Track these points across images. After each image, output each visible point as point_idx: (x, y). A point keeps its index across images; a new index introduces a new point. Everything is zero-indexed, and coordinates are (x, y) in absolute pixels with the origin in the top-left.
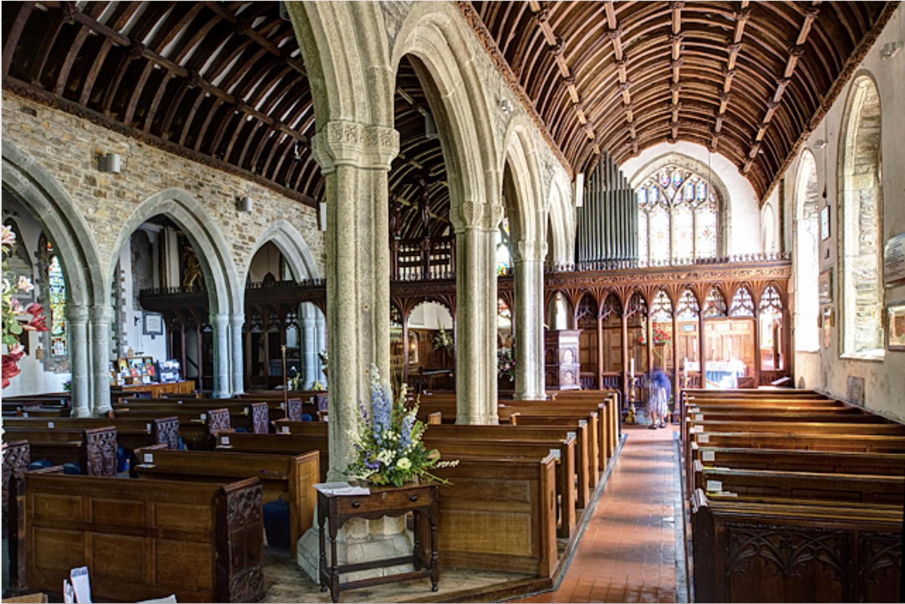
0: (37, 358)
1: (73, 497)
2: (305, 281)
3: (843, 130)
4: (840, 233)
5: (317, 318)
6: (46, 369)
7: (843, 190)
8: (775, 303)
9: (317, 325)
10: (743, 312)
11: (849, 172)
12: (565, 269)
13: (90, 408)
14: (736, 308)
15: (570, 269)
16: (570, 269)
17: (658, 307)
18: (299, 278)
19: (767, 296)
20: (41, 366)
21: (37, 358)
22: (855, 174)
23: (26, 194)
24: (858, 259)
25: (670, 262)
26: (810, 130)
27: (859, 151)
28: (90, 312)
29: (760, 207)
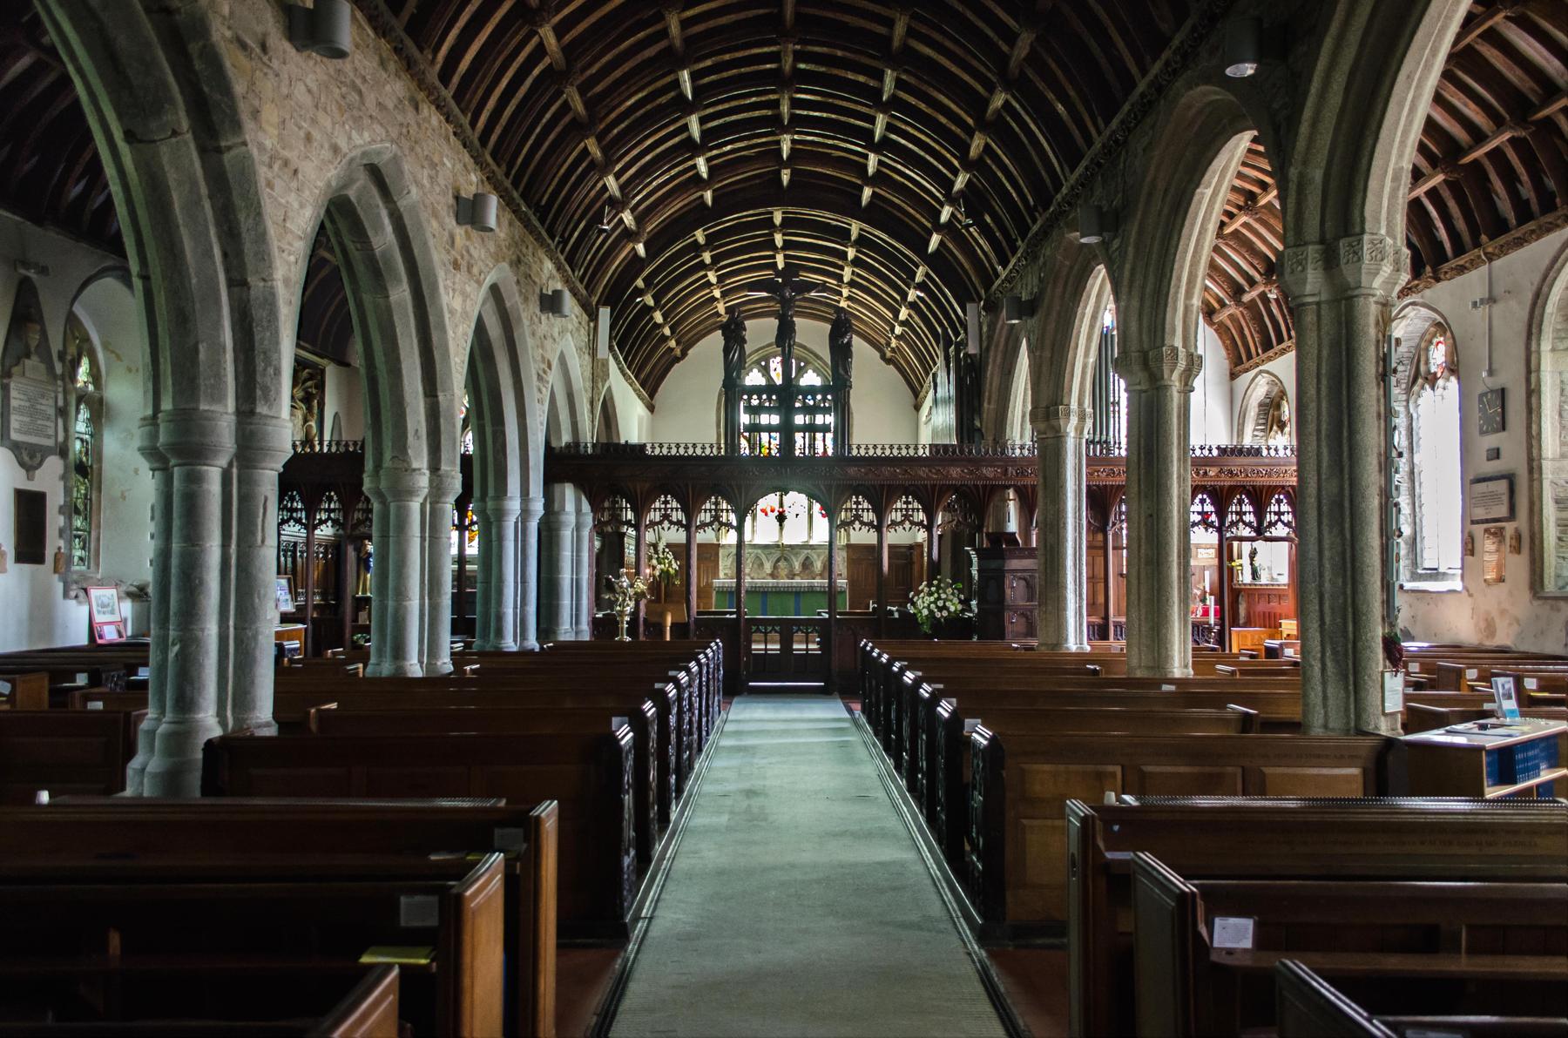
0: (55, 571)
1: (1101, 768)
2: (568, 446)
3: (1545, 289)
4: (1534, 427)
5: (578, 511)
6: (66, 595)
7: (1538, 370)
8: (1286, 518)
9: (578, 527)
10: (1280, 530)
11: (1546, 346)
12: (1018, 452)
13: (421, 662)
14: (1233, 524)
15: (1026, 452)
16: (1026, 452)
17: (1274, 518)
18: (560, 438)
19: (1274, 508)
20: (60, 586)
21: (55, 571)
22: (1553, 350)
23: (383, 253)
24: (1557, 464)
25: (916, 449)
26: (1438, 280)
27: (1560, 319)
28: (431, 481)
29: (1233, 376)
